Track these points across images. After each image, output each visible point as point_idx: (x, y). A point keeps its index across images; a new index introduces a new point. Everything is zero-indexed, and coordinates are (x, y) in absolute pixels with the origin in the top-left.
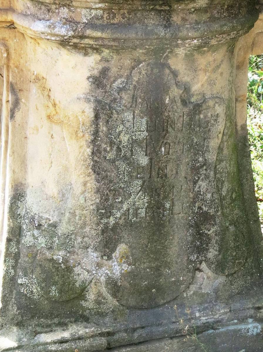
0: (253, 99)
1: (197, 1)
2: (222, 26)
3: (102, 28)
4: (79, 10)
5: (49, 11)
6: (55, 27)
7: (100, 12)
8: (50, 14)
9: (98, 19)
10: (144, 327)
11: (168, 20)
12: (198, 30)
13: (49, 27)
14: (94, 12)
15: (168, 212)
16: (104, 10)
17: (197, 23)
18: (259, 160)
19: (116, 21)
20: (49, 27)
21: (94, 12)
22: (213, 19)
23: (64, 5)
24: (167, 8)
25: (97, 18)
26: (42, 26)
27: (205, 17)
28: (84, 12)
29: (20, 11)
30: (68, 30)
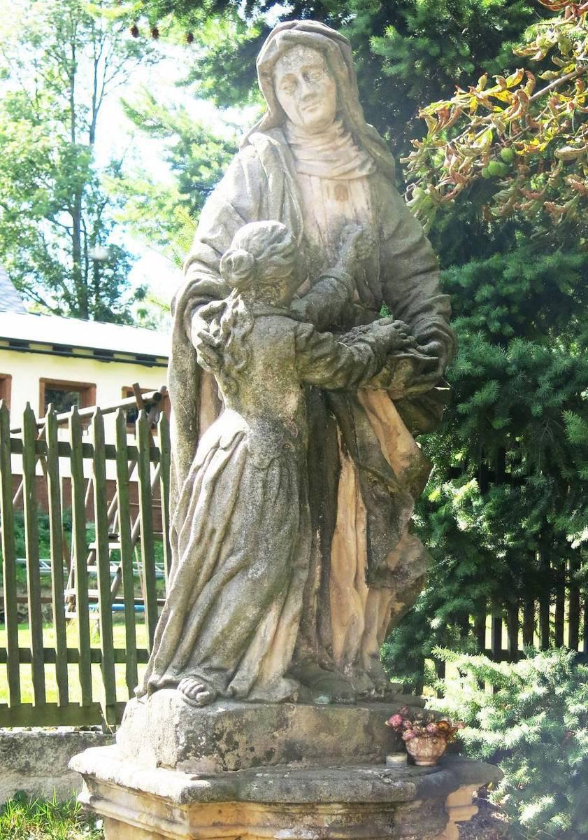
0: (277, 509)
1: (341, 3)
2: (431, 824)
3: (343, 830)
4: (321, 817)
5: (292, 820)
6: (301, 833)
7: (339, 817)
8: (294, 823)
9: (337, 823)
10: (391, 520)
11: (392, 820)
12: (415, 827)
13: (296, 833)
14: (334, 818)
15: (340, 15)
16: (342, 815)
17: (413, 822)
18: (157, 237)
19: (352, 824)
20: (296, 833)
21: (334, 818)
22: (423, 818)
23: (307, 814)
24: (393, 810)
25: (337, 822)
26: (288, 833)
27: (417, 817)
28: (326, 818)
29: (255, 824)
30: (314, 835)
